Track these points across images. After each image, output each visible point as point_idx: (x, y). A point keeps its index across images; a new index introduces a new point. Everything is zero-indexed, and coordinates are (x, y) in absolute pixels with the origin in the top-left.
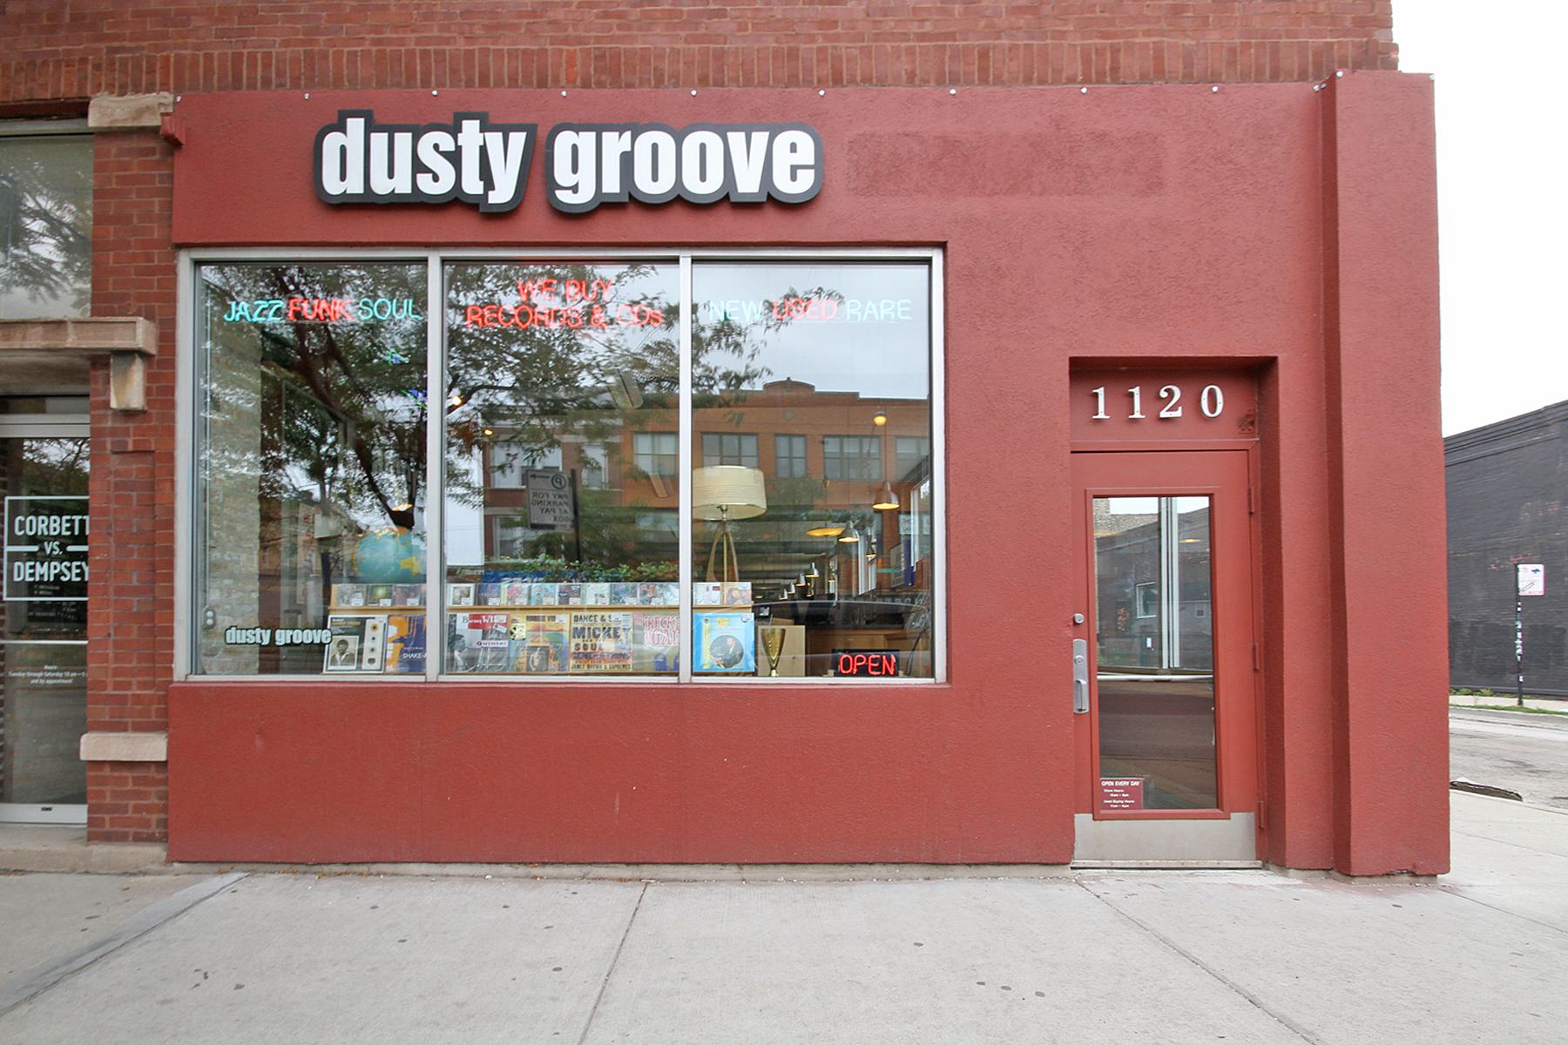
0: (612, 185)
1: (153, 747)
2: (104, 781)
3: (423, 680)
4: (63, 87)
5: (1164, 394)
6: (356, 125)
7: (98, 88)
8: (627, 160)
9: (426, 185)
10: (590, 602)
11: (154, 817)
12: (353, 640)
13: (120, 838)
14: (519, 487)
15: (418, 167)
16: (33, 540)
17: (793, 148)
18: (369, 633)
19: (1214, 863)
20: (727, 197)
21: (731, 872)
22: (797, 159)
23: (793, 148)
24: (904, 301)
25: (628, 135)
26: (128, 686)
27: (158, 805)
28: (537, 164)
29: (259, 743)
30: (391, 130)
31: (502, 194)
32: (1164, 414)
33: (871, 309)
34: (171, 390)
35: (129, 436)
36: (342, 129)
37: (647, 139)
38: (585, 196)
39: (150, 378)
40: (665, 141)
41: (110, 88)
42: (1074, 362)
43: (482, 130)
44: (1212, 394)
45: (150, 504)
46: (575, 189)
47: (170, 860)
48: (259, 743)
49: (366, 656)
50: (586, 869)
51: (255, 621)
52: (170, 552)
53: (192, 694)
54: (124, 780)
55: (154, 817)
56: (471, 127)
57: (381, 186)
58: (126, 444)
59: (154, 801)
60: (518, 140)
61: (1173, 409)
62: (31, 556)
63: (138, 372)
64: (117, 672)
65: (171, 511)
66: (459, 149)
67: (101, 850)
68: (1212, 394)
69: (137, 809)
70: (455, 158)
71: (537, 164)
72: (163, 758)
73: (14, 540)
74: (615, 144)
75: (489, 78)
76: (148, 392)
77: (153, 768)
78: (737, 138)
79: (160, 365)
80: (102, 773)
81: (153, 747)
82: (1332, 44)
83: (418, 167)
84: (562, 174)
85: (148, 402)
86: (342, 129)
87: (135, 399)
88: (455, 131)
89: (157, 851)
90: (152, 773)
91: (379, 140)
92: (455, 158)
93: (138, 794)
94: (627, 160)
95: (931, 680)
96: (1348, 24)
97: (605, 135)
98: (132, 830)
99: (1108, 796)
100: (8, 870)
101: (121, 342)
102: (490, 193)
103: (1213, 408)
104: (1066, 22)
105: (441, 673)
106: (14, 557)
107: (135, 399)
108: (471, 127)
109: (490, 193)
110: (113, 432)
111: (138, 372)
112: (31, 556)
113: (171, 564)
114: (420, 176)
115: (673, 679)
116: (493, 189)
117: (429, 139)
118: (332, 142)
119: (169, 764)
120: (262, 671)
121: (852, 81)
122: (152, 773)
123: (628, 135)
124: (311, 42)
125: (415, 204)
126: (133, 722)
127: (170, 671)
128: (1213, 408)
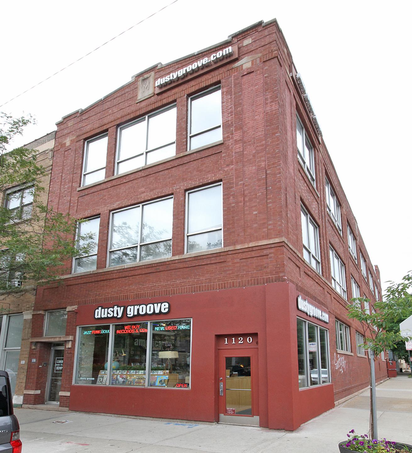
0: (136, 313)
1: (68, 394)
4: (64, 306)
5: (239, 339)
6: (100, 308)
7: (68, 306)
8: (138, 310)
9: (109, 316)
10: (140, 373)
11: (68, 404)
12: (101, 379)
13: (63, 407)
14: (384, 286)
15: (108, 313)
16: (60, 364)
17: (165, 305)
18: (104, 378)
19: (250, 425)
22: (165, 307)
23: (165, 305)
25: (138, 306)
28: (125, 311)
29: (82, 394)
30: (105, 309)
31: (120, 316)
32: (239, 342)
34: (75, 345)
36: (98, 309)
37: (141, 306)
38: (132, 315)
39: (72, 343)
40: (144, 306)
41: (70, 306)
42: (216, 335)
43: (117, 307)
44: (249, 338)
45: (71, 360)
46: (130, 314)
47: (69, 410)
48: (82, 394)
49: (103, 381)
50: (128, 416)
51: (91, 376)
52: (73, 367)
53: (74, 387)
54: (64, 398)
55: (68, 404)
56: (116, 307)
57: (103, 316)
59: (68, 401)
60: (122, 308)
61: (241, 341)
62: (59, 366)
63: (70, 343)
64: (65, 383)
65: (73, 361)
67: (60, 408)
68: (249, 338)
69: (66, 403)
70: (113, 312)
71: (125, 311)
73: (57, 364)
74: (136, 307)
76: (72, 345)
78: (156, 305)
79: (74, 342)
81: (68, 394)
82: (270, 277)
83: (108, 313)
84: (128, 312)
85: (72, 347)
86: (98, 309)
87: (70, 346)
88: (113, 308)
89: (68, 409)
90: (68, 397)
91: (103, 310)
92: (113, 312)
93: (66, 401)
94: (138, 310)
95: (308, 387)
96: (274, 273)
97: (135, 306)
98: (65, 406)
99: (228, 411)
103: (250, 341)
104: (215, 280)
105: (109, 385)
106: (57, 366)
107: (70, 346)
108: (116, 307)
110: (67, 350)
111: (70, 343)
112: (59, 366)
113: (73, 368)
114: (108, 315)
115: (144, 387)
117: (110, 309)
118: (97, 311)
120: (92, 384)
122: (68, 397)
123: (138, 306)
124: (96, 297)
125: (108, 318)
127: (72, 383)
128: (250, 341)
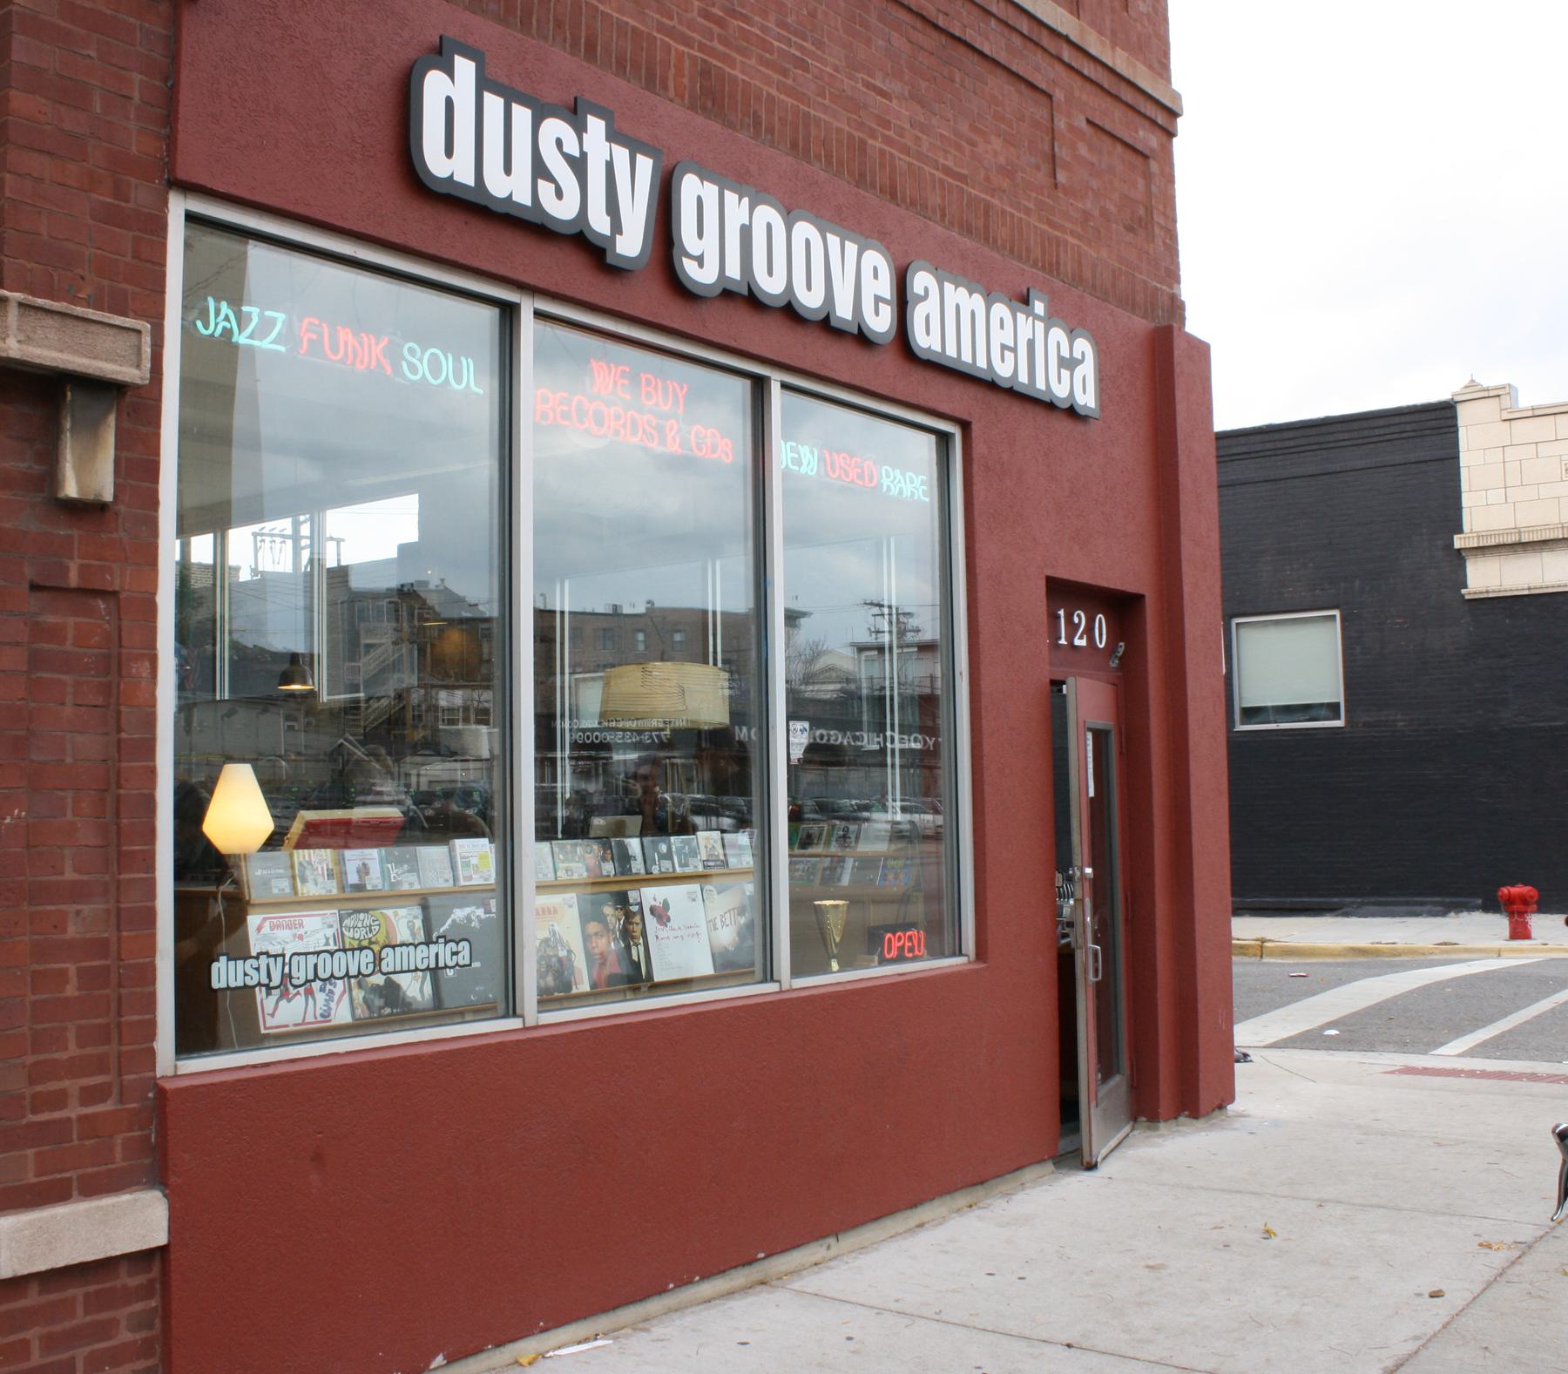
2: (28, 1318)
3: (777, 989)
20: (827, 319)
21: (961, 1199)
24: (312, 320)
26: (60, 1099)
27: (135, 1342)
33: (227, 318)
35: (72, 558)
58: (65, 570)
59: (125, 1336)
66: (584, 155)
72: (161, 1239)
75: (585, 49)
77: (34, 1289)
80: (118, 1283)
87: (104, 485)
100: (1529, 1080)
101: (55, 354)
102: (618, 236)
107: (104, 485)
109: (618, 236)
116: (621, 233)
119: (172, 1249)
121: (873, 186)
126: (80, 1178)
